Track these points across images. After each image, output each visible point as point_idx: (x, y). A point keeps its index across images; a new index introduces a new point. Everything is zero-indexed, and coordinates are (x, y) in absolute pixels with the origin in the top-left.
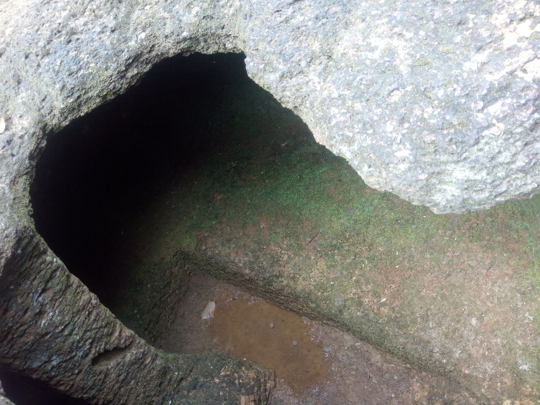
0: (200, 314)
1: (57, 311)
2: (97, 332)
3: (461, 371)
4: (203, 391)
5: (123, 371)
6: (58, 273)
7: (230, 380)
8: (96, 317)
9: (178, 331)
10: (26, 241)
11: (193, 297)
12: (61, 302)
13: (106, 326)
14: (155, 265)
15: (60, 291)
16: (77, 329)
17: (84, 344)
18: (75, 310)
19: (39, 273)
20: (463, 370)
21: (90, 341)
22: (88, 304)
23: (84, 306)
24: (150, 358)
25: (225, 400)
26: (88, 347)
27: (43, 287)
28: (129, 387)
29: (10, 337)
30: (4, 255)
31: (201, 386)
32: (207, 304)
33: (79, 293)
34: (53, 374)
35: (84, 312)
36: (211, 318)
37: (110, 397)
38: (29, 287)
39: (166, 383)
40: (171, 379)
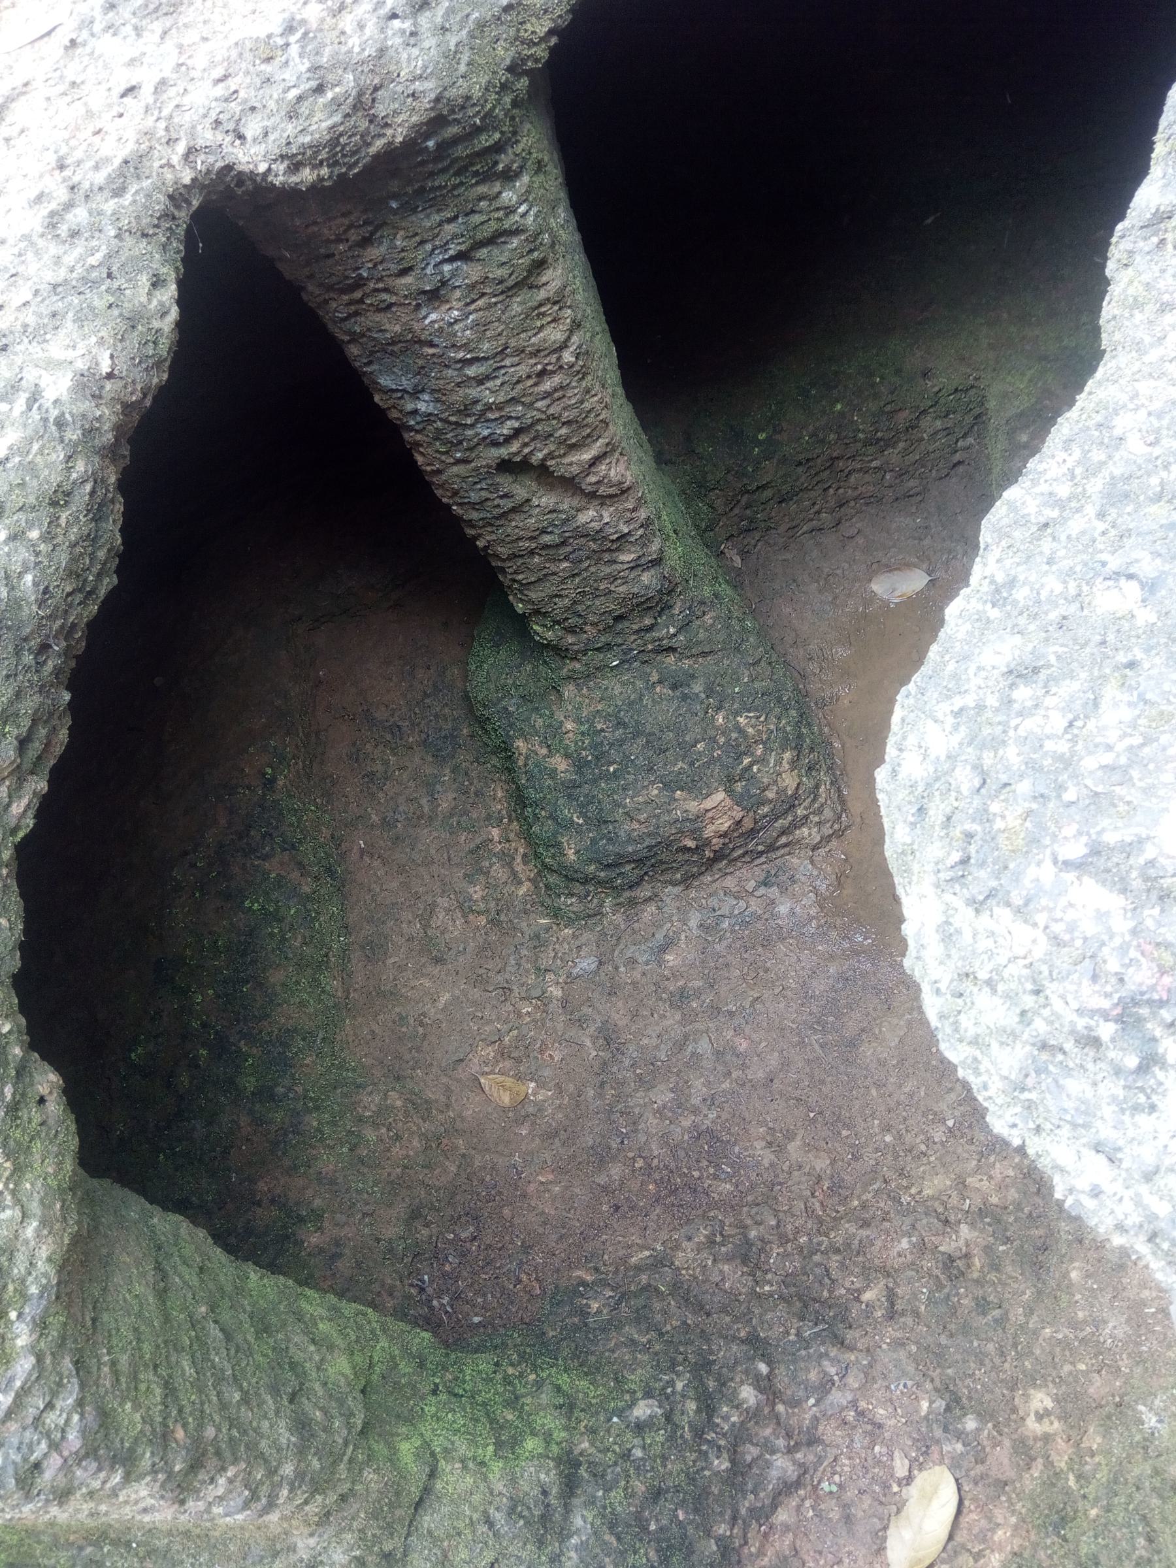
0: (876, 573)
1: (471, 317)
2: (539, 420)
3: (1072, 1260)
4: (678, 708)
5: (556, 531)
6: (515, 242)
7: (738, 745)
8: (556, 390)
9: (808, 558)
10: (454, 130)
11: (908, 520)
12: (490, 306)
13: (568, 423)
14: (898, 372)
15: (501, 282)
16: (498, 382)
17: (502, 420)
18: (513, 343)
19: (467, 215)
20: (1076, 1264)
21: (517, 425)
22: (554, 351)
23: (539, 351)
24: (632, 556)
25: (692, 764)
26: (505, 432)
27: (463, 247)
28: (553, 568)
29: (358, 295)
30: (389, 132)
31: (685, 697)
32: (909, 566)
33: (544, 314)
34: (412, 423)
35: (533, 361)
36: (885, 604)
37: (503, 551)
38: (431, 229)
39: (635, 627)
40: (650, 629)
